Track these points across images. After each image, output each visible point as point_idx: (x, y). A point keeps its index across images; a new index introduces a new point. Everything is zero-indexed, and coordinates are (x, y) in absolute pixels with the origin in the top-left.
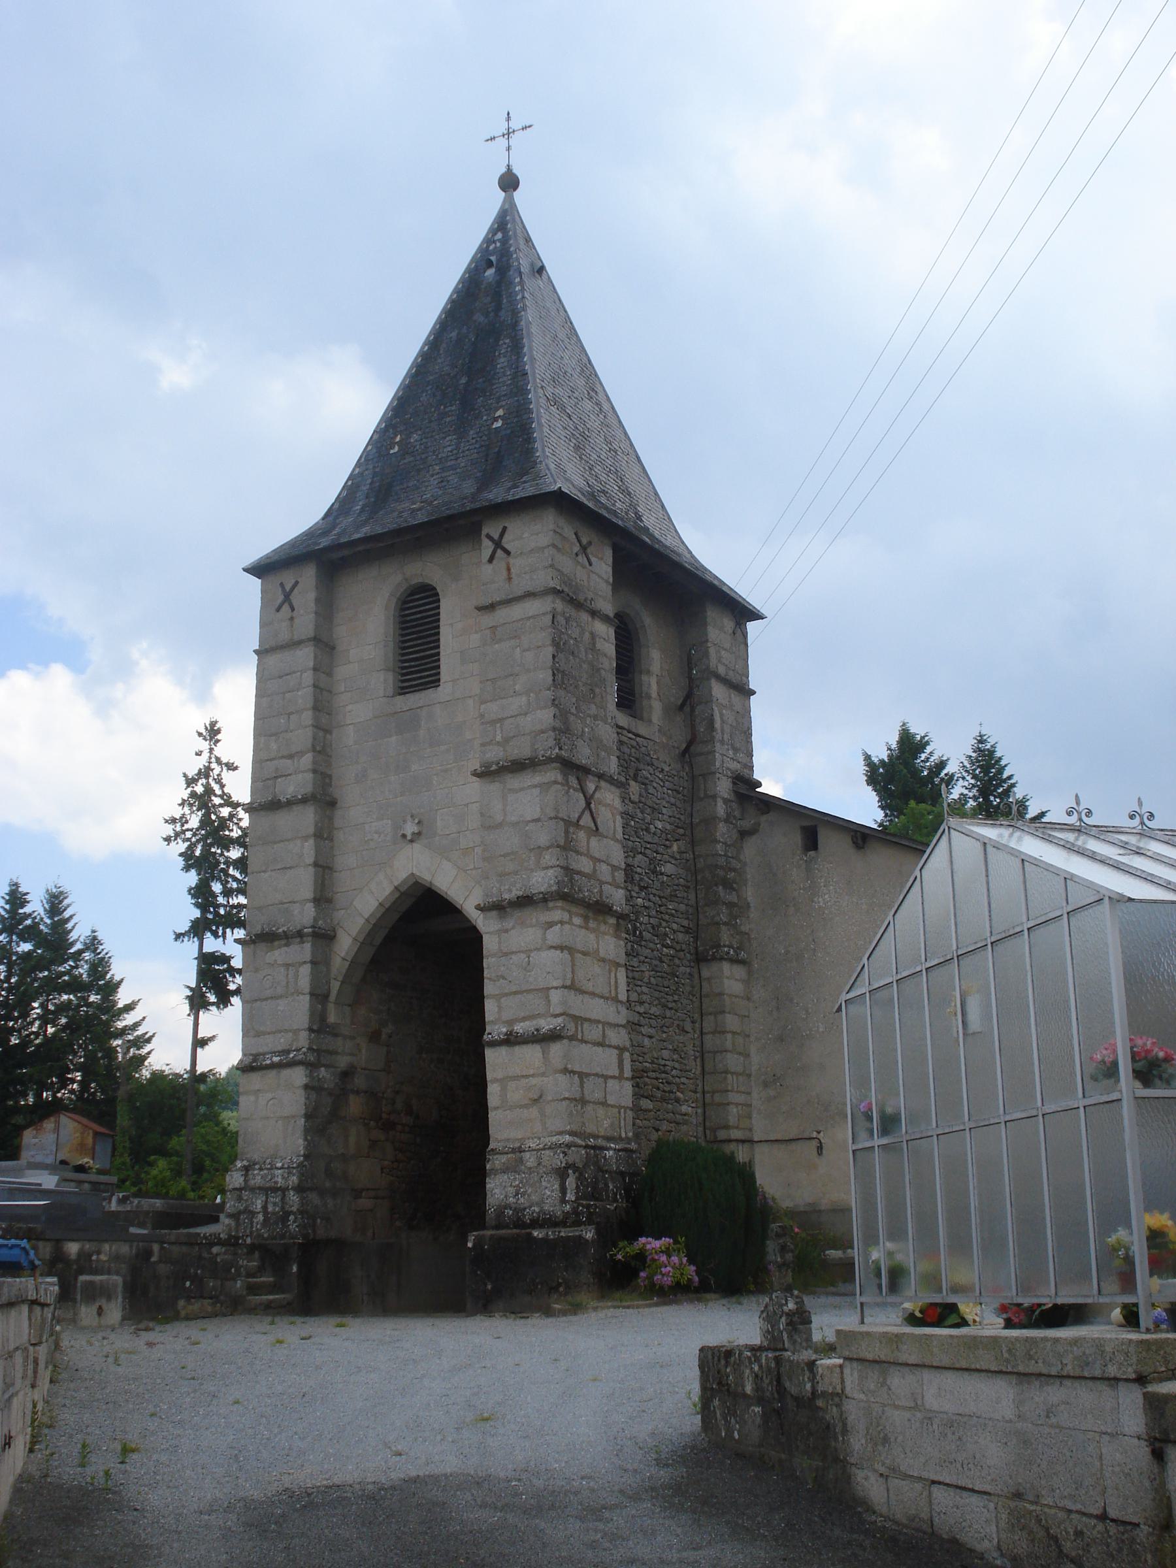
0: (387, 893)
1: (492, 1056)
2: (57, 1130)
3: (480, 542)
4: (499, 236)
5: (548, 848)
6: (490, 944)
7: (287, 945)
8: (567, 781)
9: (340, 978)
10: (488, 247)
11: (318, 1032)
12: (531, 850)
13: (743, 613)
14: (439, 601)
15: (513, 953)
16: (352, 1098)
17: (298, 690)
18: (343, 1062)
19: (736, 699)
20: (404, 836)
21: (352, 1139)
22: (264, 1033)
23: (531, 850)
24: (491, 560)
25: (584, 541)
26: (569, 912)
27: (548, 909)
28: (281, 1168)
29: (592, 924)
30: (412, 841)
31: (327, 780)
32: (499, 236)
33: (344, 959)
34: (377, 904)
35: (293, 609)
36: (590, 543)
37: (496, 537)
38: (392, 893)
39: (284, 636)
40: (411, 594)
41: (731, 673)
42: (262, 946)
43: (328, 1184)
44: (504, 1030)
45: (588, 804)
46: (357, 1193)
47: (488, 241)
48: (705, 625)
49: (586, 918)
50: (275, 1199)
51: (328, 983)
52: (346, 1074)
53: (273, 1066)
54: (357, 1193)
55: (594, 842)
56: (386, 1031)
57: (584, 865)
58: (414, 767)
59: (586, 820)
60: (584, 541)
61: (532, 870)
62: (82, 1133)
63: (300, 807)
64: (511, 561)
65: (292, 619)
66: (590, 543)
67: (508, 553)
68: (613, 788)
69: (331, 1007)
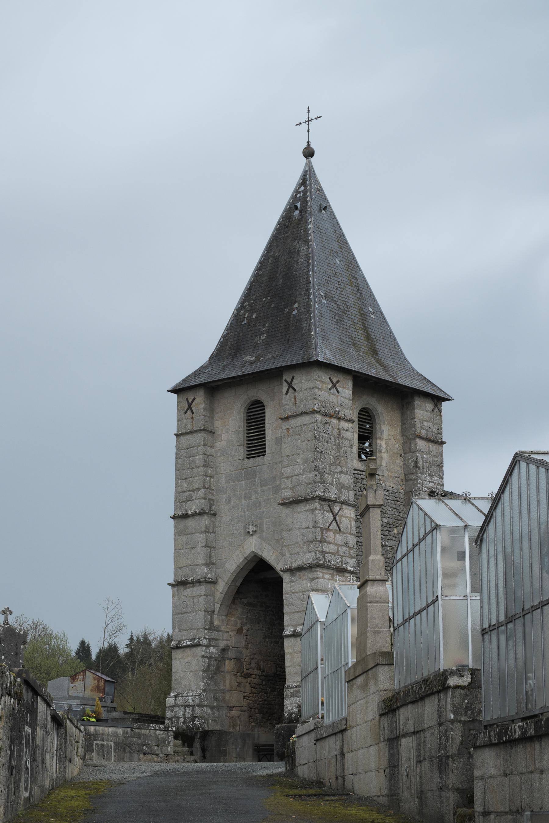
0: (241, 561)
1: (287, 643)
2: (84, 679)
3: (281, 384)
4: (302, 188)
5: (312, 542)
6: (286, 586)
7: (193, 587)
8: (323, 508)
9: (220, 603)
10: (296, 195)
11: (209, 629)
12: (305, 542)
13: (437, 399)
14: (264, 409)
15: (296, 592)
16: (227, 662)
17: (196, 456)
18: (222, 644)
19: (433, 447)
20: (249, 532)
21: (228, 682)
22: (183, 630)
23: (305, 542)
24: (287, 394)
25: (335, 381)
26: (323, 573)
27: (312, 572)
28: (192, 696)
29: (337, 578)
30: (252, 535)
31: (212, 502)
32: (302, 188)
33: (221, 593)
34: (236, 566)
35: (193, 413)
36: (338, 382)
37: (289, 381)
38: (243, 561)
39: (189, 428)
40: (252, 405)
41: (429, 434)
42: (181, 588)
43: (215, 704)
44: (292, 630)
45: (335, 518)
46: (231, 709)
47: (297, 191)
48: (414, 409)
49: (332, 575)
50: (189, 711)
51: (214, 605)
52: (224, 650)
53: (187, 646)
54: (231, 709)
55: (338, 537)
56: (245, 628)
57: (326, 548)
58: (253, 497)
59: (334, 526)
60: (335, 381)
61: (305, 553)
62: (98, 681)
63: (198, 517)
64: (297, 394)
65: (192, 418)
66: (338, 382)
67: (295, 390)
68: (350, 508)
69: (215, 617)
